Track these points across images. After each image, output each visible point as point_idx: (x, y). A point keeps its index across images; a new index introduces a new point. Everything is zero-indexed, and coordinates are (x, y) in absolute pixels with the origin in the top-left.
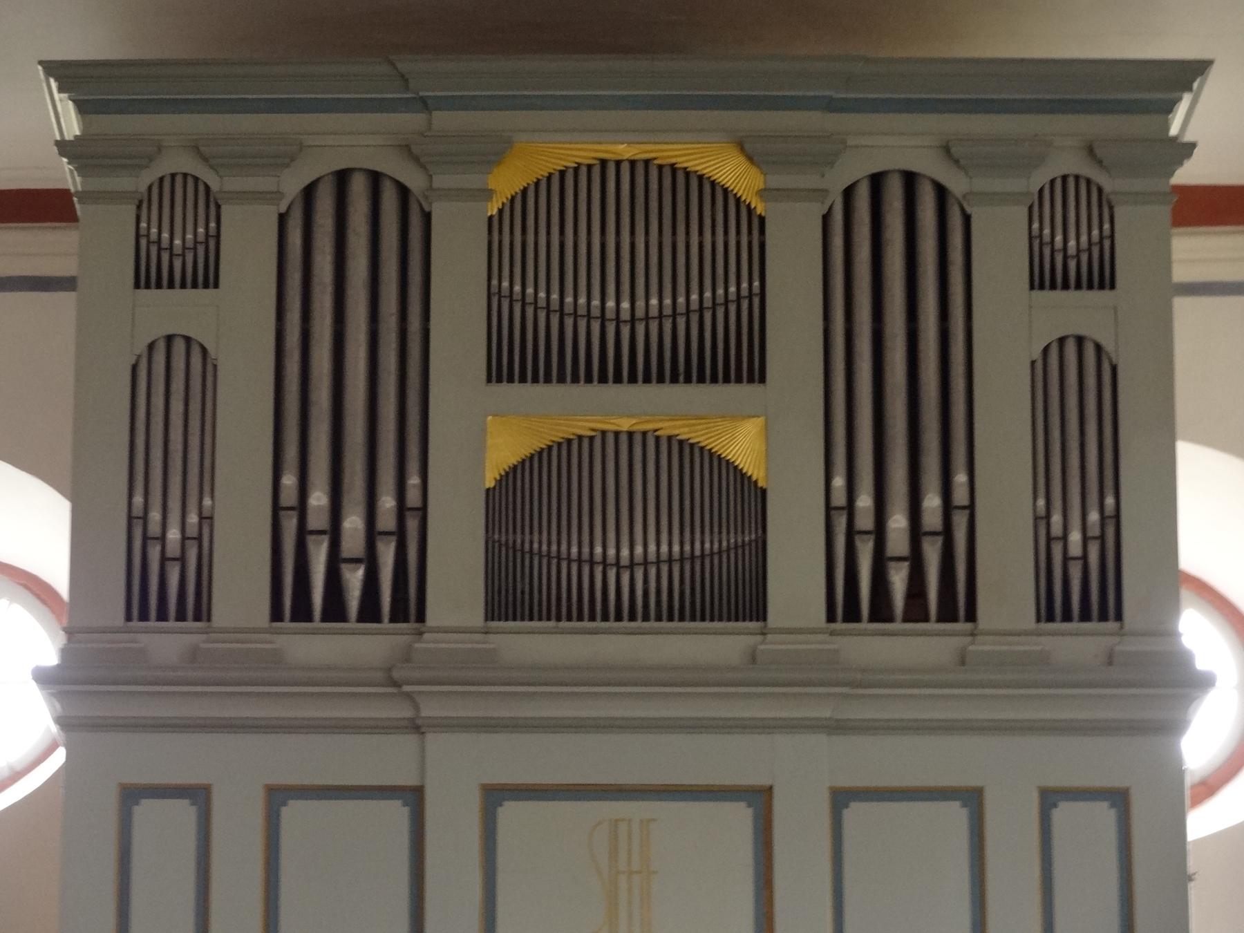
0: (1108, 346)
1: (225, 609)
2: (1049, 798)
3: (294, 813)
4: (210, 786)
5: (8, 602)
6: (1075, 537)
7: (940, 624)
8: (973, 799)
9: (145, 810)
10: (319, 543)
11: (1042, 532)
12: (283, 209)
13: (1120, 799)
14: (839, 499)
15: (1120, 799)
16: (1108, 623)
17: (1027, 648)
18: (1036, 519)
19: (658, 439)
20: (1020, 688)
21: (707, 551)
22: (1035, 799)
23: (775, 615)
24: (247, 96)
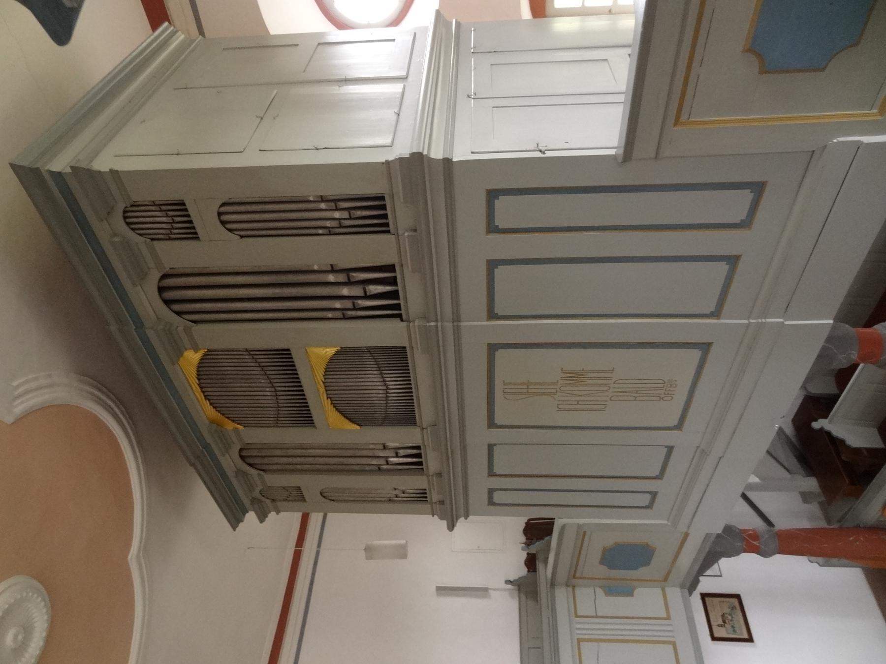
0: (220, 202)
1: (417, 441)
2: (492, 228)
3: (500, 354)
4: (488, 505)
5: (347, 77)
6: (337, 215)
7: (398, 283)
8: (493, 349)
9: (501, 221)
10: (353, 277)
11: (338, 230)
12: (150, 240)
13: (493, 195)
14: (339, 314)
15: (493, 195)
16: (399, 290)
17: (407, 244)
18: (330, 234)
19: (327, 368)
20: (431, 242)
21: (375, 363)
22: (492, 236)
23: (405, 343)
24: (97, 260)
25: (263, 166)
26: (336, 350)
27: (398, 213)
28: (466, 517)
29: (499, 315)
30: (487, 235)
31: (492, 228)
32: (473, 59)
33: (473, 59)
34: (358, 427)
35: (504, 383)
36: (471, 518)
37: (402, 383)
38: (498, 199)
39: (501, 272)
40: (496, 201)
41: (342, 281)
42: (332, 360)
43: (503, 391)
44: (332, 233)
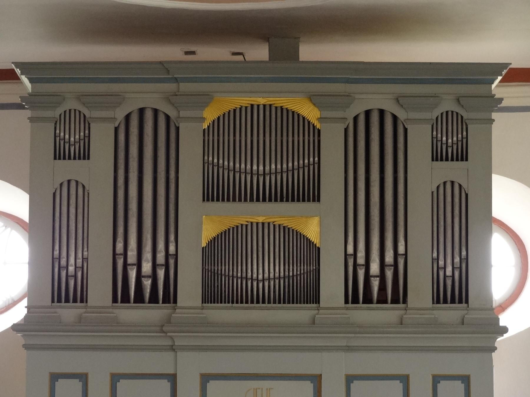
0: (464, 185)
2: (436, 379)
9: (61, 384)
13: (466, 380)
15: (466, 380)
25: (492, 228)
26: (315, 243)
27: (452, 312)
28: (26, 347)
29: (460, 382)
30: (431, 375)
31: (436, 379)
32: (26, 106)
33: (26, 106)
34: (204, 245)
35: (269, 390)
36: (24, 352)
37: (266, 291)
38: (400, 383)
39: (122, 385)
40: (460, 382)
41: (241, 167)
42: (301, 237)
43: (259, 388)
44: (433, 260)
